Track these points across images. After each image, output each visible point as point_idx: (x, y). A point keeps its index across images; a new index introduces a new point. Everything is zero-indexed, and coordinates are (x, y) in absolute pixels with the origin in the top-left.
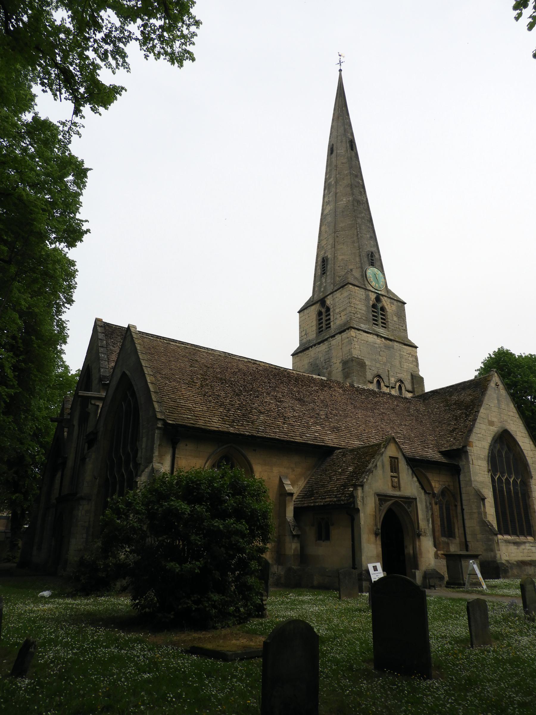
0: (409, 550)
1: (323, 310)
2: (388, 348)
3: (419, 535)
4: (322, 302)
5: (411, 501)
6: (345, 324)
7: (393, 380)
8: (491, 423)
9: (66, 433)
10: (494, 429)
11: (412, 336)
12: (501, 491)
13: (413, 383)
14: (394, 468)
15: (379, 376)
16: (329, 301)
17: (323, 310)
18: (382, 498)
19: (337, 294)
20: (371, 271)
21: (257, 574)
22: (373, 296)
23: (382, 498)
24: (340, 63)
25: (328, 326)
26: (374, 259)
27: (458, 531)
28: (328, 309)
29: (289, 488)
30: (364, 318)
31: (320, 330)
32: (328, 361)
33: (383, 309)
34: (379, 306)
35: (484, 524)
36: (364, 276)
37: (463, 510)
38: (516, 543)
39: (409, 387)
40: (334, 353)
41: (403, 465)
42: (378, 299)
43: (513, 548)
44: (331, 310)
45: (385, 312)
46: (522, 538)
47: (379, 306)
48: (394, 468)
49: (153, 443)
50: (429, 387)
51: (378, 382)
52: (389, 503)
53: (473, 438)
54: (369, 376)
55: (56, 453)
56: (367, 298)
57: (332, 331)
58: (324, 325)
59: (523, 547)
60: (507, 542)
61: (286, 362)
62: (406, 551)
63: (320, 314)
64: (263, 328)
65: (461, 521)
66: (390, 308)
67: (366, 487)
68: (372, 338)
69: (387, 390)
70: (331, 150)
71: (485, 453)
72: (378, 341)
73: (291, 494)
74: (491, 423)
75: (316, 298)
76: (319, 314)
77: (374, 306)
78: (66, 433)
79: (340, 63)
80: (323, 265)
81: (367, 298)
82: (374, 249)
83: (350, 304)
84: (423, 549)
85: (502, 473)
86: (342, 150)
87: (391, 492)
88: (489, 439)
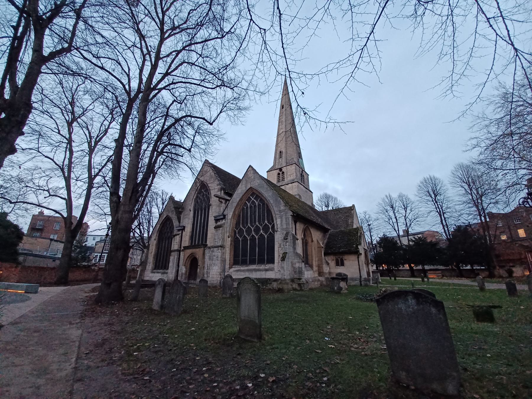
1: (281, 173)
4: (281, 169)
6: (293, 180)
16: (284, 170)
20: (300, 160)
25: (283, 179)
58: (281, 179)
63: (279, 174)
66: (305, 177)
72: (304, 188)
75: (277, 167)
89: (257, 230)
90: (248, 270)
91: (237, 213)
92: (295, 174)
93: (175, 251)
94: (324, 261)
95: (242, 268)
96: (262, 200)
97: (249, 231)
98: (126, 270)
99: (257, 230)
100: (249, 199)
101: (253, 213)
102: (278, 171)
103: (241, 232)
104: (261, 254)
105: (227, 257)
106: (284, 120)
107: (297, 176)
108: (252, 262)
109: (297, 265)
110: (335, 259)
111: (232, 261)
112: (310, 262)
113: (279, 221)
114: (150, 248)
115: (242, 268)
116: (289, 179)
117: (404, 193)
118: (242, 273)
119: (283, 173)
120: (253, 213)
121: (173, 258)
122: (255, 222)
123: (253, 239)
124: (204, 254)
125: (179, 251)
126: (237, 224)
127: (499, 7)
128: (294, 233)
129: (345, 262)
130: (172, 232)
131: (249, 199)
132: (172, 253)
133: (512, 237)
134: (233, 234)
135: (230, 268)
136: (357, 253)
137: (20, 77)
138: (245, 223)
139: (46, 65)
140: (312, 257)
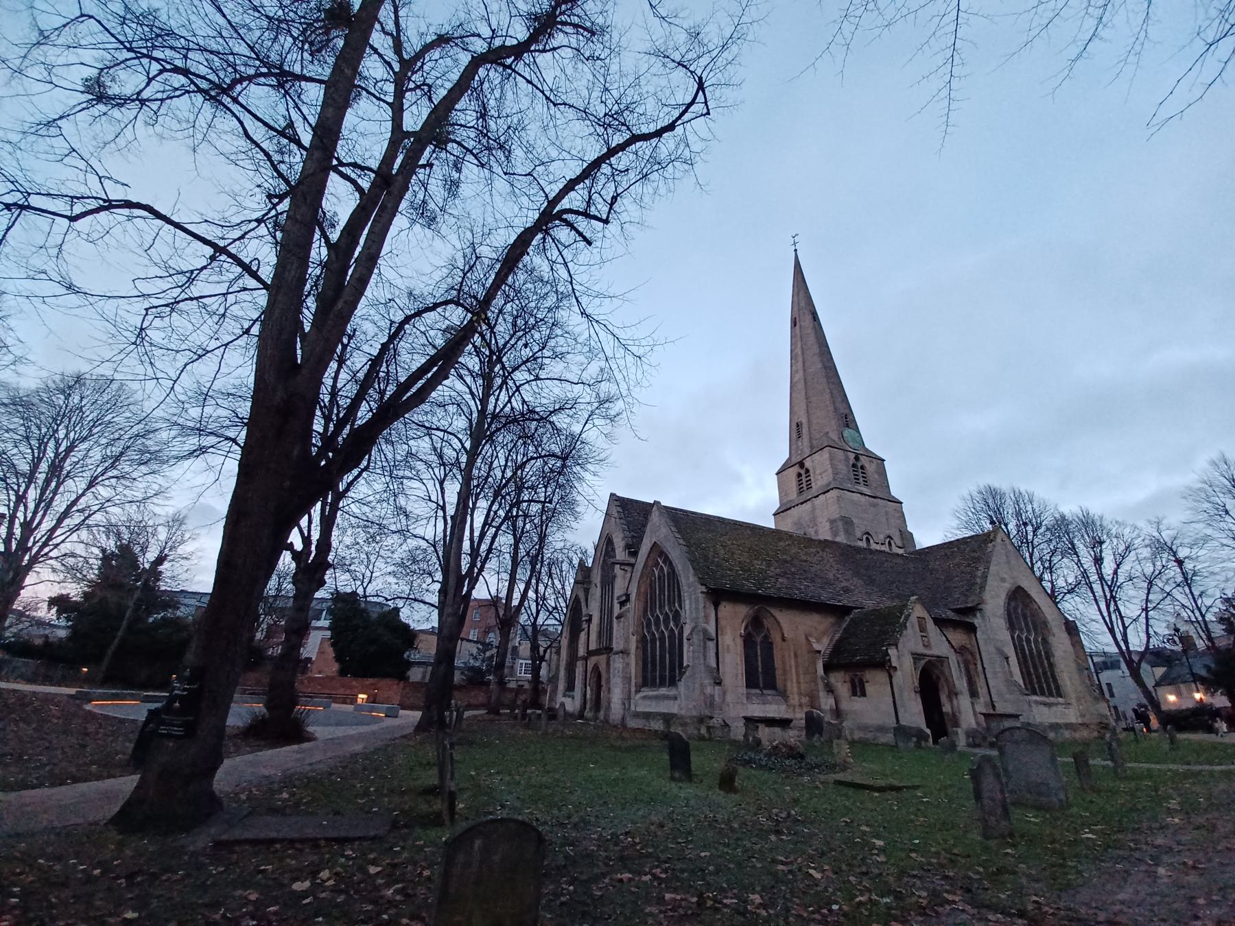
0: (946, 708)
1: (803, 472)
2: (875, 505)
3: (956, 694)
4: (801, 464)
5: (941, 660)
6: (828, 485)
7: (882, 537)
10: (1007, 586)
11: (895, 492)
12: (1023, 650)
13: (902, 539)
14: (923, 629)
15: (868, 533)
16: (808, 464)
17: (803, 472)
18: (917, 657)
19: (816, 456)
20: (847, 433)
21: (400, 759)
22: (852, 456)
23: (917, 657)
24: (795, 244)
25: (809, 487)
27: (982, 690)
28: (807, 471)
29: (817, 647)
31: (801, 491)
32: (814, 520)
33: (862, 467)
34: (859, 465)
37: (984, 669)
38: (1045, 704)
39: (899, 543)
40: (818, 512)
41: (930, 625)
42: (857, 458)
43: (1045, 709)
45: (864, 470)
46: (1052, 700)
47: (859, 465)
48: (923, 629)
51: (868, 539)
52: (923, 662)
53: (987, 596)
54: (858, 535)
55: (575, 617)
56: (847, 459)
57: (814, 491)
59: (1054, 708)
60: (1037, 702)
61: (770, 523)
62: (944, 710)
63: (799, 475)
64: (747, 492)
65: (983, 680)
66: (871, 468)
67: (900, 646)
68: (856, 496)
69: (878, 547)
70: (794, 323)
71: (1001, 611)
72: (863, 499)
73: (819, 652)
74: (1003, 580)
75: (795, 460)
76: (796, 473)
77: (854, 466)
79: (795, 244)
80: (797, 429)
81: (847, 459)
82: (847, 411)
84: (962, 709)
85: (1021, 630)
86: (807, 321)
87: (921, 650)
88: (1003, 596)
90: (656, 698)
91: (642, 590)
92: (830, 470)
94: (821, 686)
95: (651, 693)
98: (261, 597)
102: (796, 469)
106: (799, 351)
107: (835, 474)
108: (662, 684)
109: (709, 690)
110: (848, 679)
111: (640, 680)
112: (779, 683)
113: (687, 602)
115: (651, 693)
116: (820, 483)
117: (1002, 483)
118: (654, 703)
124: (608, 664)
128: (711, 629)
129: (869, 688)
132: (903, 722)
134: (640, 630)
135: (637, 691)
136: (884, 665)
139: (328, 629)
140: (785, 672)
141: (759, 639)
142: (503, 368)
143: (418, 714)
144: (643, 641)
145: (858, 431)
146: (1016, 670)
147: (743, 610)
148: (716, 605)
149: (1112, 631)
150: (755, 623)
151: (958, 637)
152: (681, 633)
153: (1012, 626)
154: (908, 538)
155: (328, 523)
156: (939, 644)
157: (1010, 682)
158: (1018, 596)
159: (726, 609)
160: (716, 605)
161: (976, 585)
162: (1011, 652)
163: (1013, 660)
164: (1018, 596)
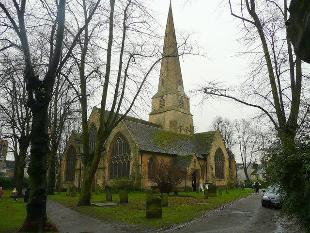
4: (162, 97)
8: (216, 146)
9: (34, 97)
10: (217, 148)
17: (162, 100)
20: (180, 87)
26: (180, 82)
27: (205, 177)
30: (67, 100)
31: (160, 107)
32: (164, 120)
33: (183, 101)
35: (212, 175)
36: (177, 89)
42: (181, 98)
44: (165, 101)
49: (123, 166)
50: (197, 131)
61: (146, 118)
63: (161, 101)
68: (179, 113)
74: (216, 146)
77: (180, 101)
78: (34, 97)
83: (170, 100)
87: (194, 168)
89: (118, 159)
93: (77, 170)
96: (125, 140)
97: (118, 159)
99: (122, 159)
100: (119, 139)
101: (120, 148)
103: (114, 159)
104: (124, 174)
105: (107, 174)
114: (62, 166)
119: (164, 100)
120: (120, 148)
121: (77, 174)
122: (121, 154)
123: (120, 164)
125: (80, 170)
126: (112, 155)
127: (146, 77)
130: (75, 157)
131: (119, 139)
133: (233, 186)
137: (13, 11)
138: (116, 154)
141: (152, 165)
142: (64, 75)
143: (41, 78)
144: (111, 164)
145: (183, 86)
146: (214, 172)
147: (149, 156)
148: (142, 155)
149: (243, 159)
150: (151, 160)
151: (202, 163)
152: (129, 163)
153: (215, 160)
154: (192, 128)
155: (81, 46)
156: (198, 167)
157: (212, 175)
158: (219, 151)
159: (144, 156)
160: (142, 155)
161: (208, 148)
162: (214, 167)
163: (214, 169)
164: (219, 151)
